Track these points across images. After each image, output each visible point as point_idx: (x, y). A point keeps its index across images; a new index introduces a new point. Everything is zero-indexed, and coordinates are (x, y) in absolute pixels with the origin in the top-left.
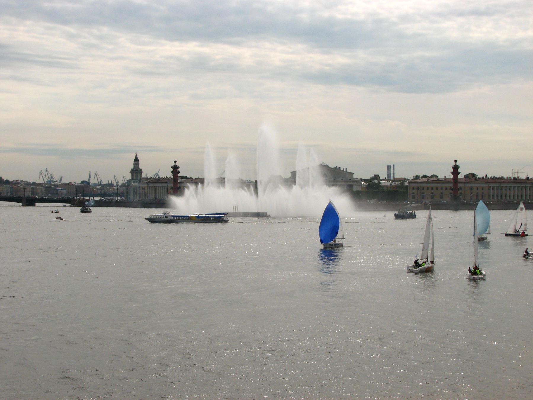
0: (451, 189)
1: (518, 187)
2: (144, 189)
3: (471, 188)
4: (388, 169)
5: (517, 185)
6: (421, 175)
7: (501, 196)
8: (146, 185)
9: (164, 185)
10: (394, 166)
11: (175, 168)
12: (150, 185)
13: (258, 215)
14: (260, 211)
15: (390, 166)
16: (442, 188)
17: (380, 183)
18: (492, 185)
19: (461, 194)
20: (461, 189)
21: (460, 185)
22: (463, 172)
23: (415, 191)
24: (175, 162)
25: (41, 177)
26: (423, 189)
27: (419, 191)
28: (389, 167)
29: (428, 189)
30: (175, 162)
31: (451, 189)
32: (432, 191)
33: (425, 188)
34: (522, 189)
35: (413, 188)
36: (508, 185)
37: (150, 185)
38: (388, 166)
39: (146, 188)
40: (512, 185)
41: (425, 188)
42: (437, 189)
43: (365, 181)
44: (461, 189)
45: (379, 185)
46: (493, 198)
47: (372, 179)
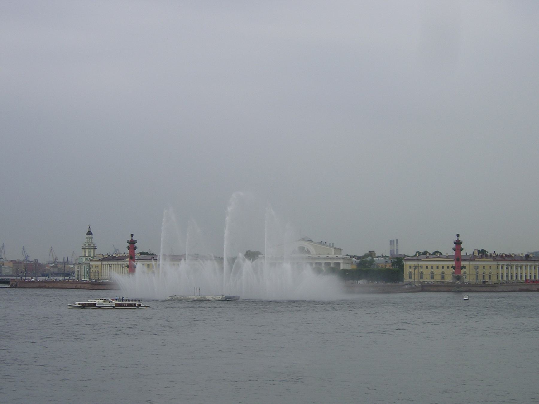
0: (454, 268)
1: (531, 266)
2: (98, 267)
3: (477, 267)
4: (391, 244)
5: (529, 263)
6: (422, 251)
7: (512, 276)
8: (100, 263)
9: (119, 263)
10: (397, 240)
11: (132, 243)
12: (103, 263)
13: (228, 299)
14: (227, 293)
15: (393, 240)
16: (432, 267)
17: (373, 260)
18: (501, 263)
19: (465, 273)
20: (464, 267)
21: (463, 263)
22: (468, 249)
23: (412, 270)
24: (132, 235)
25: (51, 254)
26: (421, 267)
27: (416, 270)
28: (392, 242)
29: (438, 267)
30: (458, 235)
31: (454, 268)
32: (443, 270)
33: (424, 267)
34: (535, 268)
35: (410, 267)
36: (520, 263)
37: (103, 263)
38: (391, 241)
39: (100, 267)
40: (524, 263)
41: (435, 267)
42: (438, 267)
43: (359, 258)
44: (464, 267)
45: (372, 262)
46: (502, 279)
47: (366, 256)
